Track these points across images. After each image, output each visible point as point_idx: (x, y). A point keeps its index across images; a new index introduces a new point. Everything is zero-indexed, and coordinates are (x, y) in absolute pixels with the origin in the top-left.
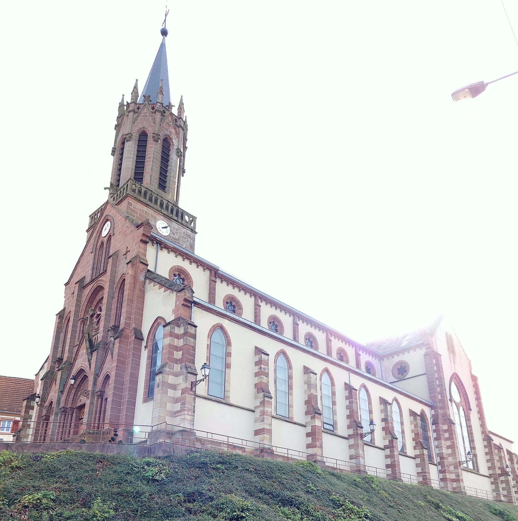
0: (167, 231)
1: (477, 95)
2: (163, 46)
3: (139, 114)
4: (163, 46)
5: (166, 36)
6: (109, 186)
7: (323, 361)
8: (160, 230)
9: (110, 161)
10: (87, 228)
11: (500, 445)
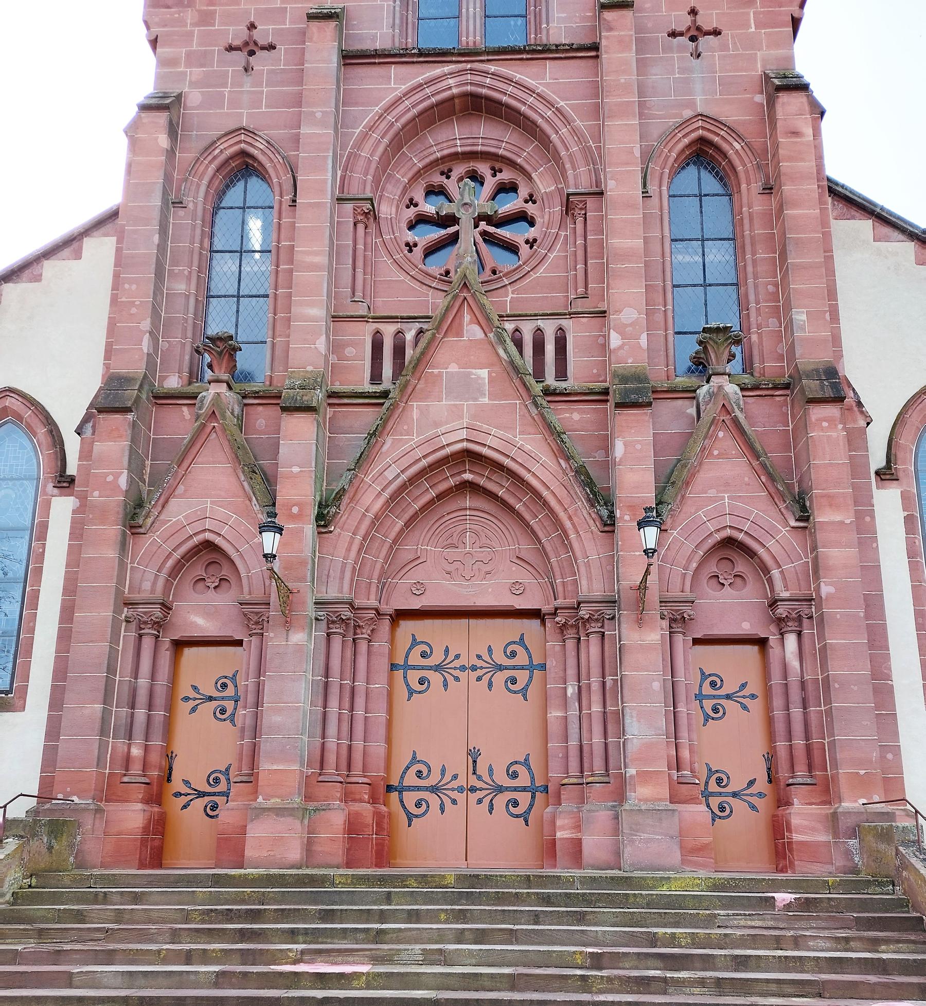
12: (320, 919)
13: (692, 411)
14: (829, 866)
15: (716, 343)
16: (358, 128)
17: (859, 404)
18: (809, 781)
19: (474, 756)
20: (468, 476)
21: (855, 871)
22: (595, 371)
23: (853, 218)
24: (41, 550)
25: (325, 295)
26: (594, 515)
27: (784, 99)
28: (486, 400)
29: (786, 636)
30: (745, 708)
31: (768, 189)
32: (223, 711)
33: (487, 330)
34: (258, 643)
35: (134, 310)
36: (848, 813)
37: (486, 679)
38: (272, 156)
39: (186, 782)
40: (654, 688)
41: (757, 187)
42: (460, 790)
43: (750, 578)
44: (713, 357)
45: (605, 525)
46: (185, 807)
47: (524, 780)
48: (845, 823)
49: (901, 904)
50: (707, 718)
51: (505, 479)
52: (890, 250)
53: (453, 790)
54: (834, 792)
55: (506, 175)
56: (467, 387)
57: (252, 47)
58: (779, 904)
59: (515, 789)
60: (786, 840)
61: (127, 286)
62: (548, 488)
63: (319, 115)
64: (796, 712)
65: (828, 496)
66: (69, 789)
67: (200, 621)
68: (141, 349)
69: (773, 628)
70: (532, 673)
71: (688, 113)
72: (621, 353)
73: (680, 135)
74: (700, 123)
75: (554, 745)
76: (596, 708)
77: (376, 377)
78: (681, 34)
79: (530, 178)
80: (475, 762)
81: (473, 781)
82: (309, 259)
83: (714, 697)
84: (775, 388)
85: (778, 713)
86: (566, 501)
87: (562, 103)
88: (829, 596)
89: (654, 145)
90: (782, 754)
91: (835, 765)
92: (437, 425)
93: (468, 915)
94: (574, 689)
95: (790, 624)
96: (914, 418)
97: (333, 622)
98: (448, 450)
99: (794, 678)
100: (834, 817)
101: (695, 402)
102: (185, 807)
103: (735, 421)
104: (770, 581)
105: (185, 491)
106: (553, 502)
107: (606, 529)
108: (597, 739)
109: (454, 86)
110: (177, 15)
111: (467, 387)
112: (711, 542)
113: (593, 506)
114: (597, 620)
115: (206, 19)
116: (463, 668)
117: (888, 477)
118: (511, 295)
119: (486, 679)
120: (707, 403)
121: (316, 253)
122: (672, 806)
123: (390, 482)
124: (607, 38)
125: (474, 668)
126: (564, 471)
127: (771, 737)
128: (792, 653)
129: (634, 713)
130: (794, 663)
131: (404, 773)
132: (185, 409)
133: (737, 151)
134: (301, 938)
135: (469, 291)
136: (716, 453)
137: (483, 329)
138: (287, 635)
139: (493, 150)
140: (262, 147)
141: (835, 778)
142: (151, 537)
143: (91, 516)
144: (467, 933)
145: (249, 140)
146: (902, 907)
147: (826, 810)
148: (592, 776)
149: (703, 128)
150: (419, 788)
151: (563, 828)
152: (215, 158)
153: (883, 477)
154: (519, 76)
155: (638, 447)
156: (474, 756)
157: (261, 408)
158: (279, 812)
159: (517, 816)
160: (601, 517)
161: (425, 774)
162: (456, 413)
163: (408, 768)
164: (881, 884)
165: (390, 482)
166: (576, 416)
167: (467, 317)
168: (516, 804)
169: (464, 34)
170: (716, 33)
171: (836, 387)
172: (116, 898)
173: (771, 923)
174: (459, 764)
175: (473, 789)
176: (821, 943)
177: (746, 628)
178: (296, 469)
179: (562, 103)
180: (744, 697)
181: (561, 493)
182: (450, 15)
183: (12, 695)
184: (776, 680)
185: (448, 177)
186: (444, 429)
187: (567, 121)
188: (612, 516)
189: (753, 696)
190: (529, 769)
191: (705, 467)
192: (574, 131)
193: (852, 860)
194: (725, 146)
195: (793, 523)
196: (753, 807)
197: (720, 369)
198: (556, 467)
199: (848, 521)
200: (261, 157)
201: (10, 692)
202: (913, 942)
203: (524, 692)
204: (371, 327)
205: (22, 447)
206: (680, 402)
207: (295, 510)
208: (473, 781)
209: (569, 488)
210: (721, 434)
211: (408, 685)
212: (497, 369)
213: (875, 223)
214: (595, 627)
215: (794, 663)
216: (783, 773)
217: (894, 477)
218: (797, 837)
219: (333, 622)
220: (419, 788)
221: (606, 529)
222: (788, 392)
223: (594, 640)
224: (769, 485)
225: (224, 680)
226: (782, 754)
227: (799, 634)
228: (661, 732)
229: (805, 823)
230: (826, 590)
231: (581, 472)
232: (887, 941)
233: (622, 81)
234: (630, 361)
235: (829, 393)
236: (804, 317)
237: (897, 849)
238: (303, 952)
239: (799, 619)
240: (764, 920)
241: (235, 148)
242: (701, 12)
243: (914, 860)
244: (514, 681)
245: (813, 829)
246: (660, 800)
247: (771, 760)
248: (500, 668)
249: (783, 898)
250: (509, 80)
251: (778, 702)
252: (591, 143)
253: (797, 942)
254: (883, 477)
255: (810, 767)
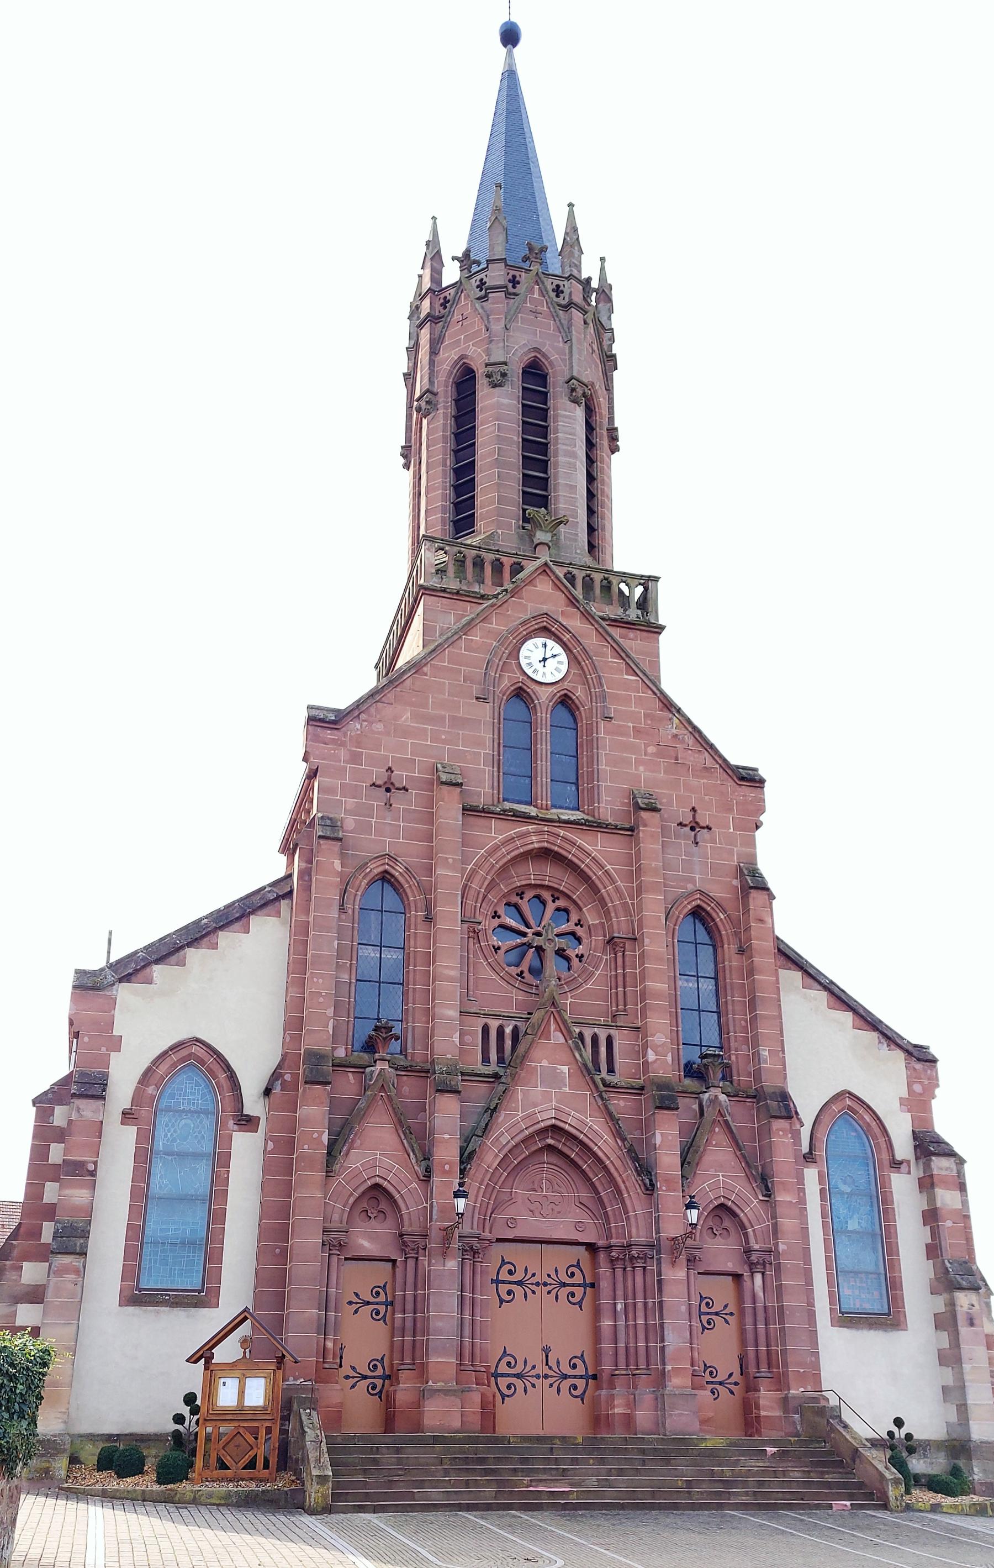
0: (560, 666)
1: (31, 1155)
2: (510, 78)
3: (453, 304)
4: (510, 78)
5: (514, 46)
6: (460, 255)
7: (881, 1022)
8: (533, 669)
9: (403, 392)
10: (408, 314)
11: (880, 1042)
12: (521, 1463)
13: (696, 1107)
14: (781, 1432)
15: (714, 1065)
16: (469, 865)
17: (797, 1113)
18: (769, 1375)
19: (546, 1351)
20: (550, 1141)
21: (798, 1435)
22: (633, 1071)
23: (789, 969)
24: (226, 1176)
25: (459, 1001)
26: (640, 1182)
27: (754, 894)
28: (567, 1089)
29: (755, 1274)
30: (727, 1322)
31: (741, 951)
32: (378, 1313)
33: (568, 1039)
34: (413, 1265)
35: (321, 1000)
36: (794, 1398)
37: (554, 1292)
38: (408, 878)
39: (353, 1368)
40: (682, 1310)
41: (734, 947)
42: (538, 1377)
43: (732, 1230)
44: (711, 1073)
45: (647, 1190)
46: (353, 1387)
47: (580, 1370)
48: (792, 1404)
49: (830, 1453)
50: (704, 1328)
51: (576, 1146)
52: (812, 995)
53: (532, 1376)
54: (784, 1383)
55: (561, 903)
56: (553, 1079)
57: (388, 785)
58: (769, 1454)
59: (575, 1377)
60: (754, 1415)
61: (315, 980)
62: (609, 1158)
63: (450, 861)
64: (761, 1326)
65: (783, 1183)
66: (297, 1374)
67: (366, 1244)
68: (328, 1031)
69: (746, 1267)
70: (585, 1289)
71: (690, 887)
72: (655, 1065)
73: (534, 623)
74: (698, 896)
75: (606, 1346)
76: (640, 1321)
77: (486, 1060)
78: (685, 825)
79: (580, 909)
80: (547, 1356)
81: (546, 1370)
82: (447, 972)
83: (708, 1314)
84: (748, 1097)
85: (749, 1327)
86: (621, 1170)
87: (609, 867)
88: (783, 1250)
89: (668, 907)
90: (751, 1355)
91: (785, 1364)
92: (535, 1105)
93: (606, 1460)
94: (622, 1305)
95: (758, 1267)
96: (826, 1119)
97: (466, 1251)
98: (542, 1125)
99: (760, 1305)
100: (785, 1400)
101: (697, 1101)
102: (353, 1387)
103: (726, 1122)
104: (746, 1235)
105: (361, 1144)
106: (612, 1170)
107: (648, 1192)
108: (641, 1344)
109: (535, 842)
110: (333, 752)
111: (553, 1079)
112: (712, 1206)
113: (639, 1175)
114: (642, 1258)
115: (355, 758)
116: (537, 1284)
117: (810, 1160)
118: (570, 1000)
119: (554, 1292)
120: (708, 1107)
121: (452, 968)
122: (694, 1392)
123: (504, 1146)
124: (643, 831)
125: (545, 1284)
126: (620, 1148)
127: (743, 1342)
128: (759, 1287)
129: (670, 1328)
130: (760, 1294)
131: (498, 1363)
132: (350, 1074)
133: (721, 919)
134: (520, 1474)
135: (556, 1008)
136: (714, 1143)
137: (564, 1035)
138: (444, 1261)
139: (556, 886)
140: (401, 871)
141: (786, 1374)
142: (338, 1179)
143: (303, 1164)
144: (613, 1470)
145: (391, 863)
146: (831, 1455)
147: (779, 1395)
148: (637, 1369)
149: (700, 899)
150: (508, 1375)
151: (618, 1406)
152: (367, 874)
153: (807, 1160)
154: (580, 841)
155: (670, 1138)
156: (546, 1351)
157: (405, 1078)
158: (446, 1392)
159: (576, 1397)
160: (645, 1185)
161: (513, 1365)
162: (547, 1097)
163: (500, 1360)
164: (818, 1442)
165: (504, 1146)
166: (622, 1103)
167: (553, 1027)
168: (575, 1387)
169: (539, 798)
170: (709, 828)
171: (787, 1107)
172: (384, 1451)
173: (768, 1464)
174: (536, 1358)
175: (546, 1377)
176: (797, 1474)
177: (730, 1266)
178: (447, 1136)
179: (609, 867)
180: (726, 1314)
181: (618, 1163)
182: (526, 775)
183: (204, 1294)
184: (748, 1305)
185: (522, 898)
186: (539, 1108)
187: (613, 882)
188: (652, 1185)
189: (732, 1314)
190: (584, 1362)
191: (708, 1152)
192: (617, 889)
193: (796, 1428)
194: (714, 915)
195: (761, 1198)
196: (732, 1393)
197: (716, 1083)
198: (614, 1144)
199: (794, 1201)
200: (400, 879)
201: (199, 1292)
202: (840, 1473)
203: (580, 1304)
204: (481, 1022)
205: (198, 1084)
206: (688, 1099)
207: (447, 1167)
208: (546, 1370)
209: (623, 1160)
210: (717, 1130)
211: (499, 1296)
212: (574, 1066)
213: (804, 975)
214: (640, 1263)
215: (760, 1294)
216: (752, 1370)
217: (814, 1161)
218: (763, 1413)
219: (466, 1251)
220: (508, 1375)
221: (648, 1192)
222: (755, 1100)
223: (639, 1271)
224: (747, 1170)
225: (377, 1289)
226: (751, 1355)
227: (763, 1274)
228: (686, 1341)
229: (768, 1403)
230: (782, 1247)
231: (631, 1150)
232: (828, 1473)
233: (653, 865)
234: (661, 1072)
235: (784, 1114)
236: (767, 1053)
237: (828, 1420)
238: (531, 1481)
239: (764, 1264)
240: (764, 1462)
241: (381, 869)
242: (699, 811)
243: (838, 1427)
244: (573, 1295)
245: (772, 1408)
246: (686, 1387)
247: (742, 1359)
248: (564, 1285)
249: (770, 1450)
250: (573, 844)
251: (749, 1319)
252: (628, 900)
253: (784, 1473)
254: (807, 1160)
255: (769, 1366)
